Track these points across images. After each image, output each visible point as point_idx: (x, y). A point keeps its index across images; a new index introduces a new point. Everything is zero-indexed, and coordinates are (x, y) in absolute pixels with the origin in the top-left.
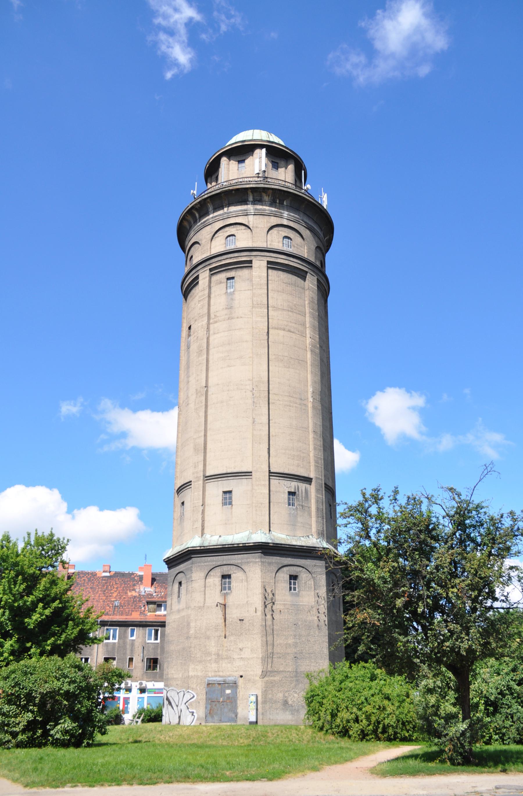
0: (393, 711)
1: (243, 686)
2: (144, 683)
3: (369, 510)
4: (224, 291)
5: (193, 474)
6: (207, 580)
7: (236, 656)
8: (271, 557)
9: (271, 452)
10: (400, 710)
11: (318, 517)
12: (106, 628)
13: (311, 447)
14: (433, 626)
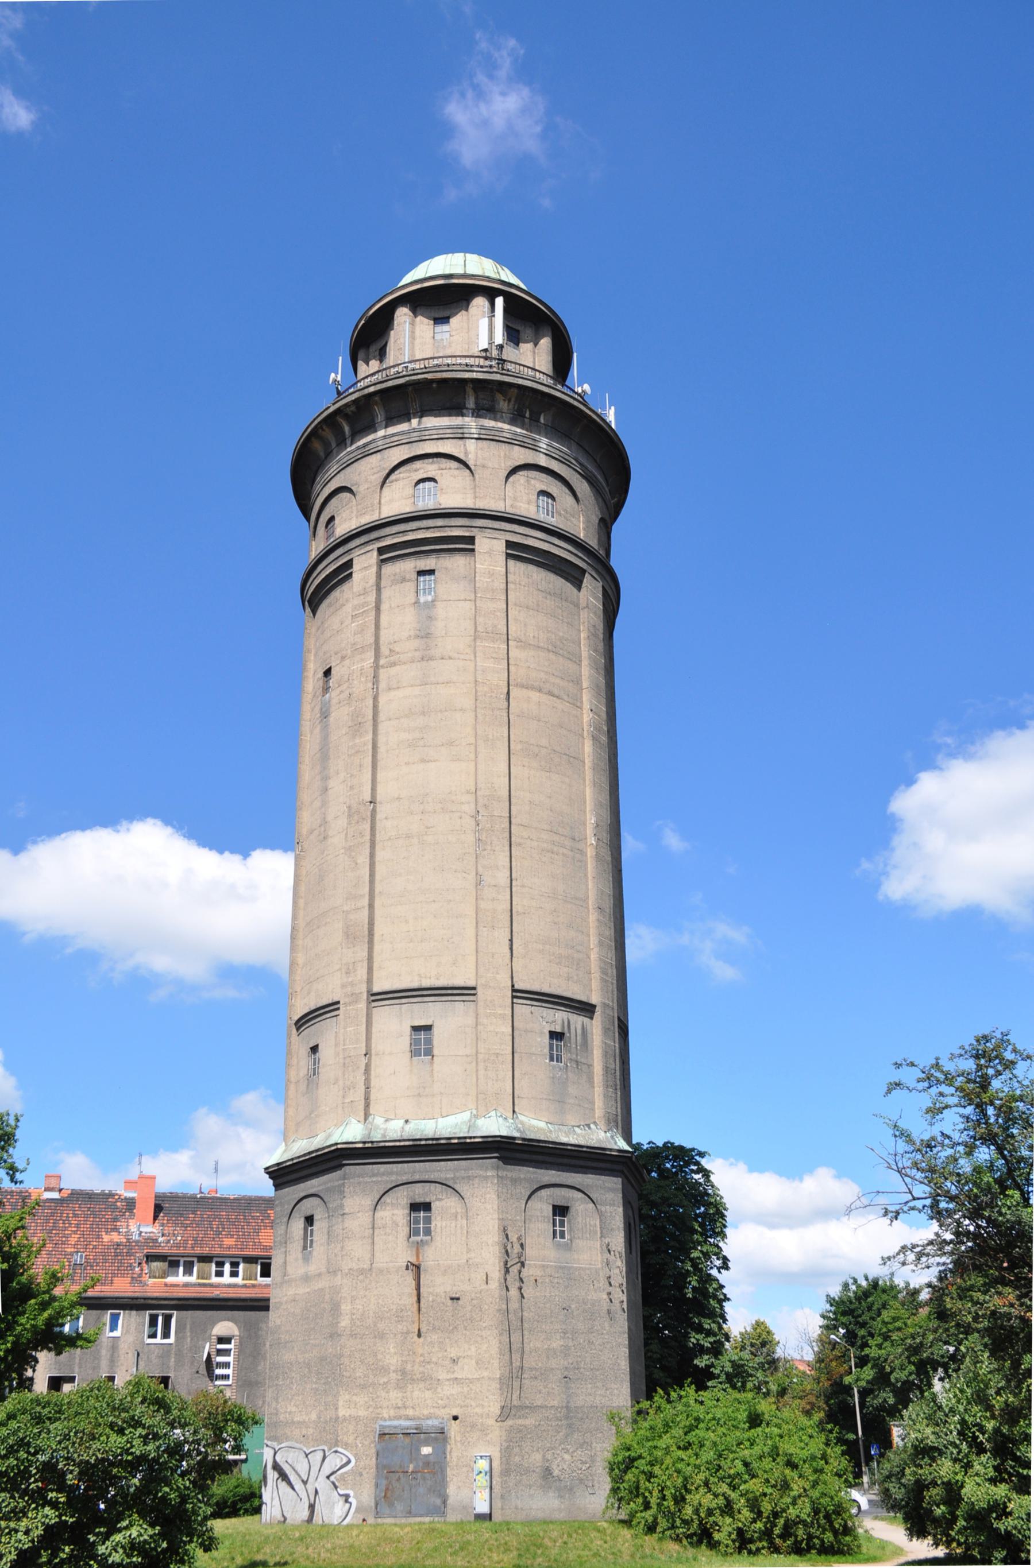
0: (805, 1490)
1: (458, 1439)
5: (343, 986)
6: (378, 1214)
7: (443, 1375)
9: (514, 947)
13: (593, 941)
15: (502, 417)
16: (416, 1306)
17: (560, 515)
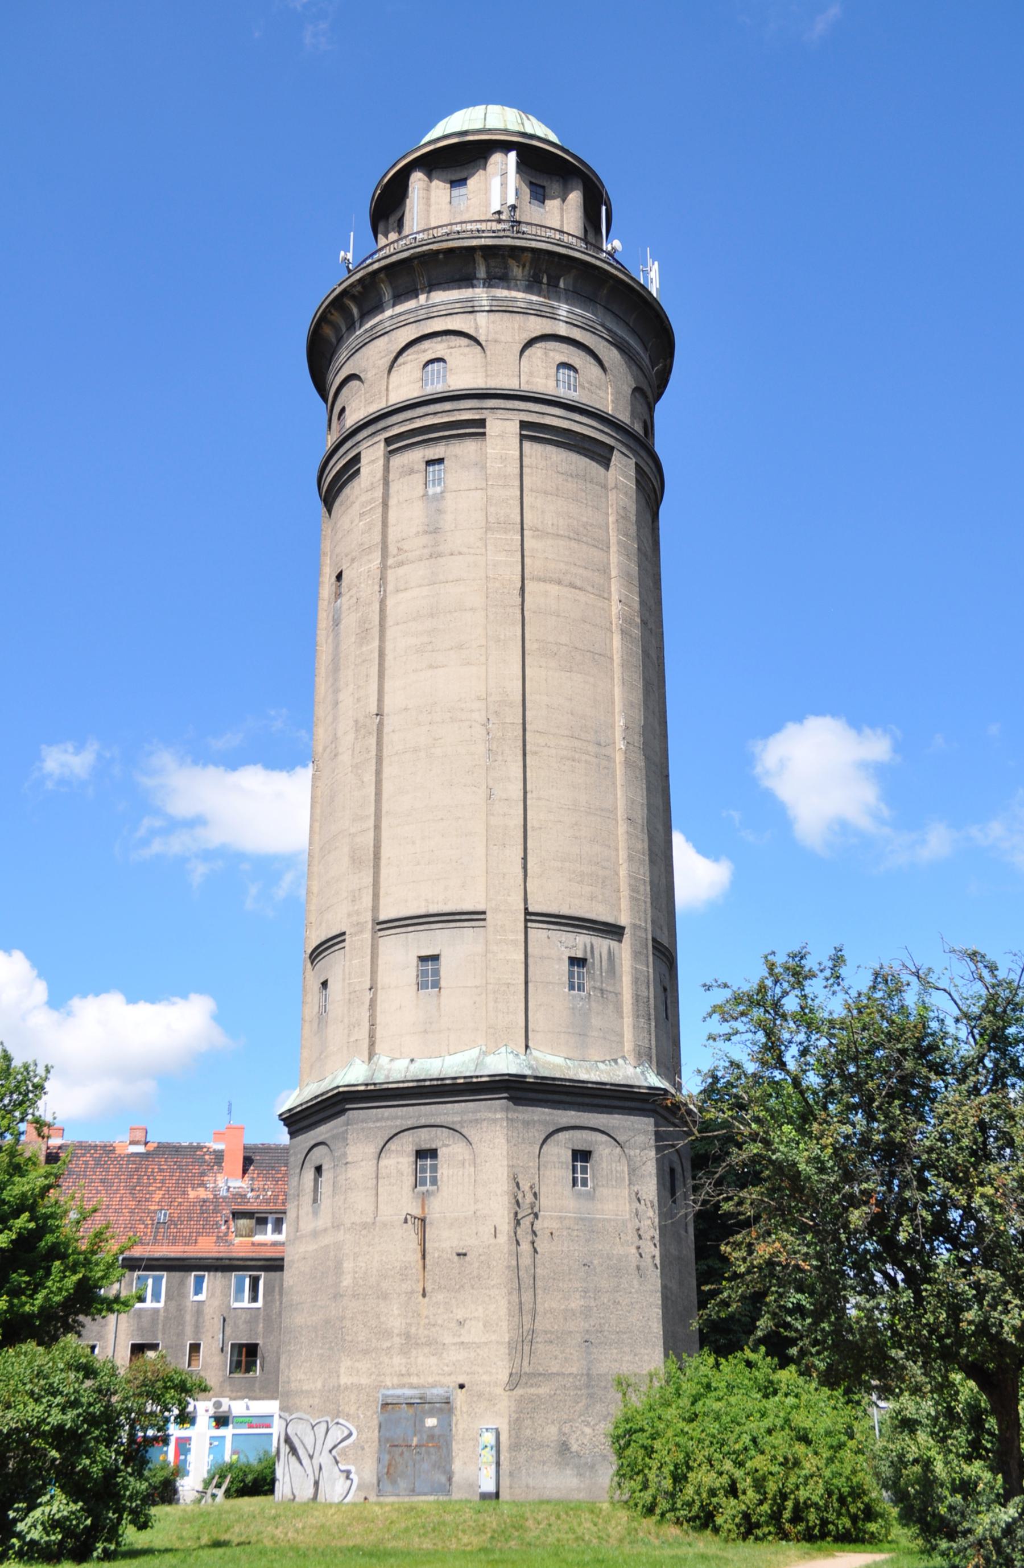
2: (225, 1402)
3: (783, 1001)
4: (420, 490)
5: (349, 915)
6: (383, 1162)
7: (448, 1339)
8: (530, 1108)
10: (835, 1467)
11: (637, 1016)
12: (136, 1274)
13: (623, 855)
14: (935, 1272)
15: (516, 285)
16: (421, 1263)
17: (583, 388)
